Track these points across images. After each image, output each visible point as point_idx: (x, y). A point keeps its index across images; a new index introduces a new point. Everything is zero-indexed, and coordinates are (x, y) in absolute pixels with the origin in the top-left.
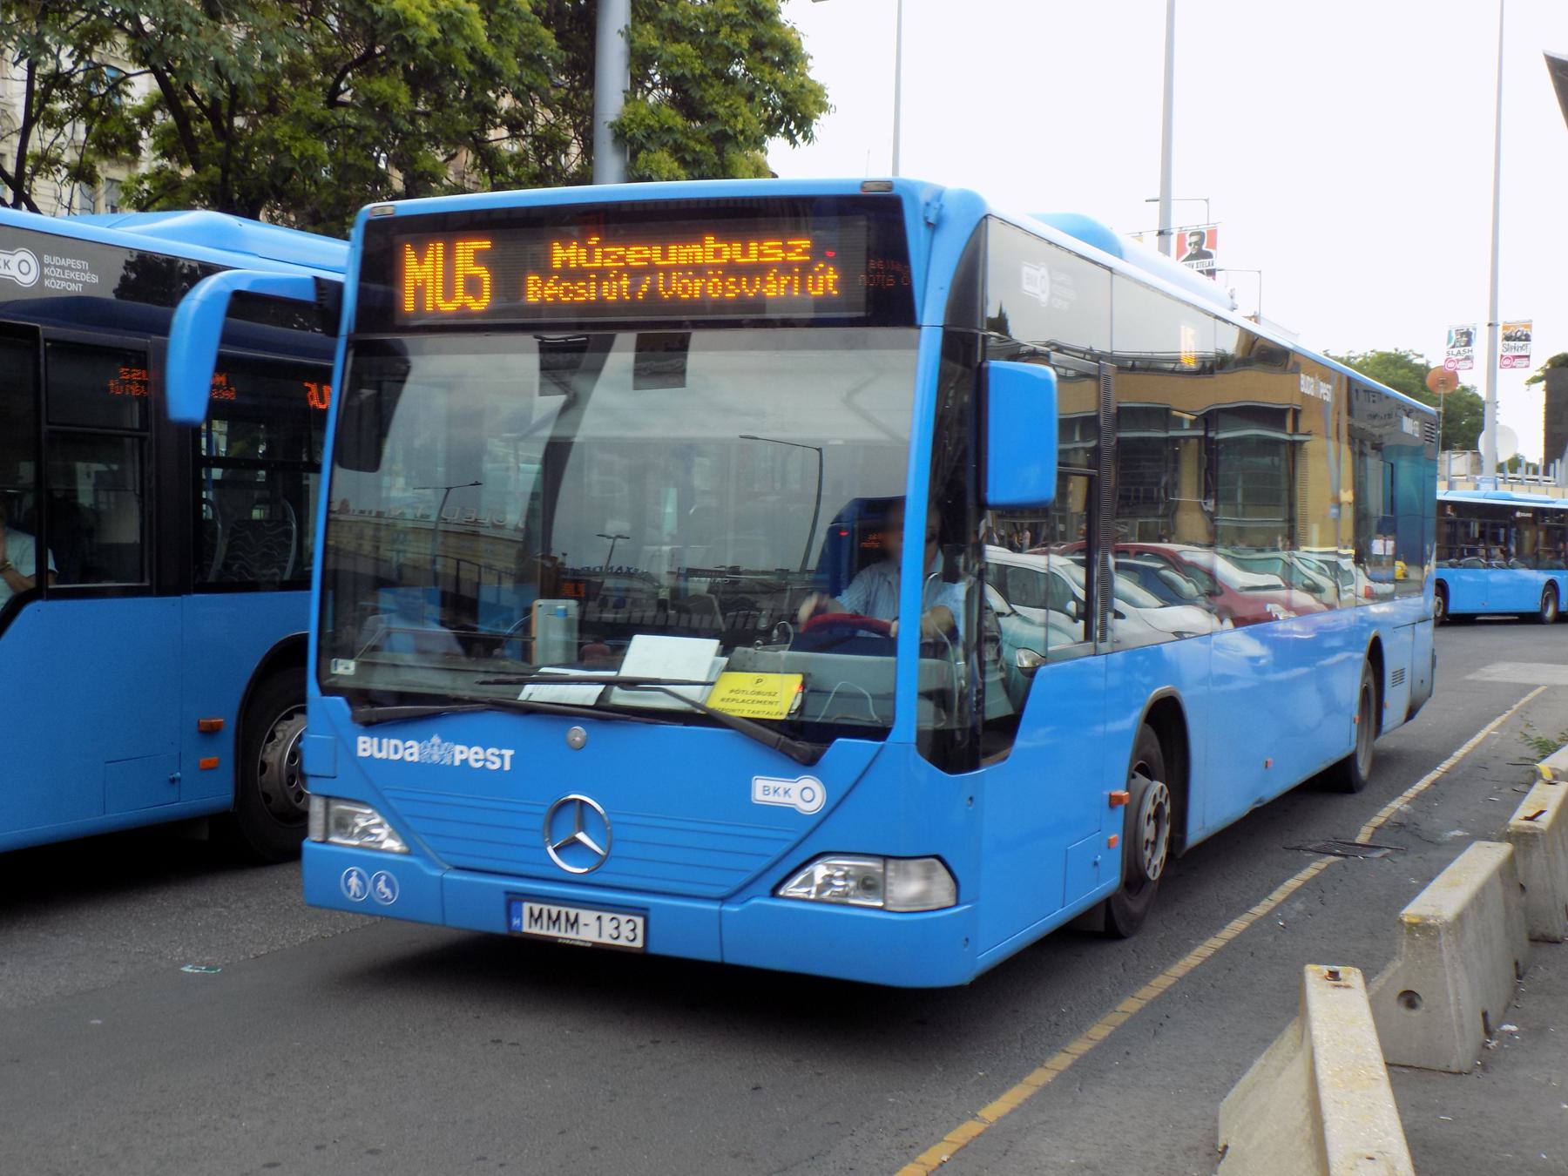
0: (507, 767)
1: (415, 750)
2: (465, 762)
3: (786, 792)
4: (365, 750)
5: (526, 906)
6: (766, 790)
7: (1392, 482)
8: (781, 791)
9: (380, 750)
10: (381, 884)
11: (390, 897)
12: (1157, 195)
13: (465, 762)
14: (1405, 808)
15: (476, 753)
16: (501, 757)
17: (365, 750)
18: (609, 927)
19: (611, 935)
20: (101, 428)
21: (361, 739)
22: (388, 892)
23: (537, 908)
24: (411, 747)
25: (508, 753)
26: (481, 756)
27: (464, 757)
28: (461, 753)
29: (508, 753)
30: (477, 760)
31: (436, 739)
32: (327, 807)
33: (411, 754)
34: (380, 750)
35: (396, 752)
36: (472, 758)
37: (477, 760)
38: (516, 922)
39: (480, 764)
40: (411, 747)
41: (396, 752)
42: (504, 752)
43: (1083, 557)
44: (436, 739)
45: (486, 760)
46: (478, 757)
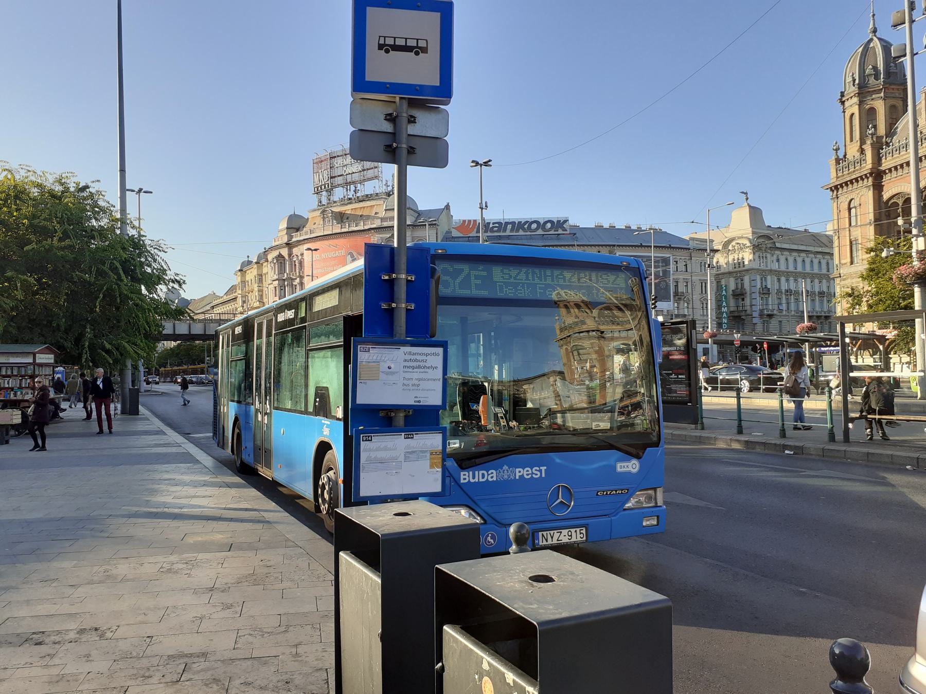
0: (543, 476)
1: (494, 475)
2: (522, 477)
3: (627, 466)
4: (465, 479)
5: (540, 533)
6: (621, 467)
7: (622, 246)
8: (626, 467)
9: (474, 478)
10: (489, 539)
11: (493, 543)
12: (386, 43)
13: (522, 477)
14: (460, 399)
15: (528, 471)
16: (540, 471)
17: (465, 479)
18: (556, 535)
19: (568, 539)
20: (375, 348)
21: (462, 473)
22: (492, 541)
23: (545, 533)
24: (492, 473)
25: (543, 468)
26: (530, 472)
27: (521, 474)
28: (519, 472)
29: (543, 468)
30: (528, 475)
31: (505, 467)
32: (656, 503)
33: (492, 477)
34: (474, 478)
35: (483, 477)
36: (525, 473)
37: (528, 475)
38: (536, 542)
39: (530, 476)
40: (492, 473)
41: (483, 477)
42: (541, 468)
43: (851, 374)
44: (505, 467)
45: (533, 473)
46: (528, 473)
